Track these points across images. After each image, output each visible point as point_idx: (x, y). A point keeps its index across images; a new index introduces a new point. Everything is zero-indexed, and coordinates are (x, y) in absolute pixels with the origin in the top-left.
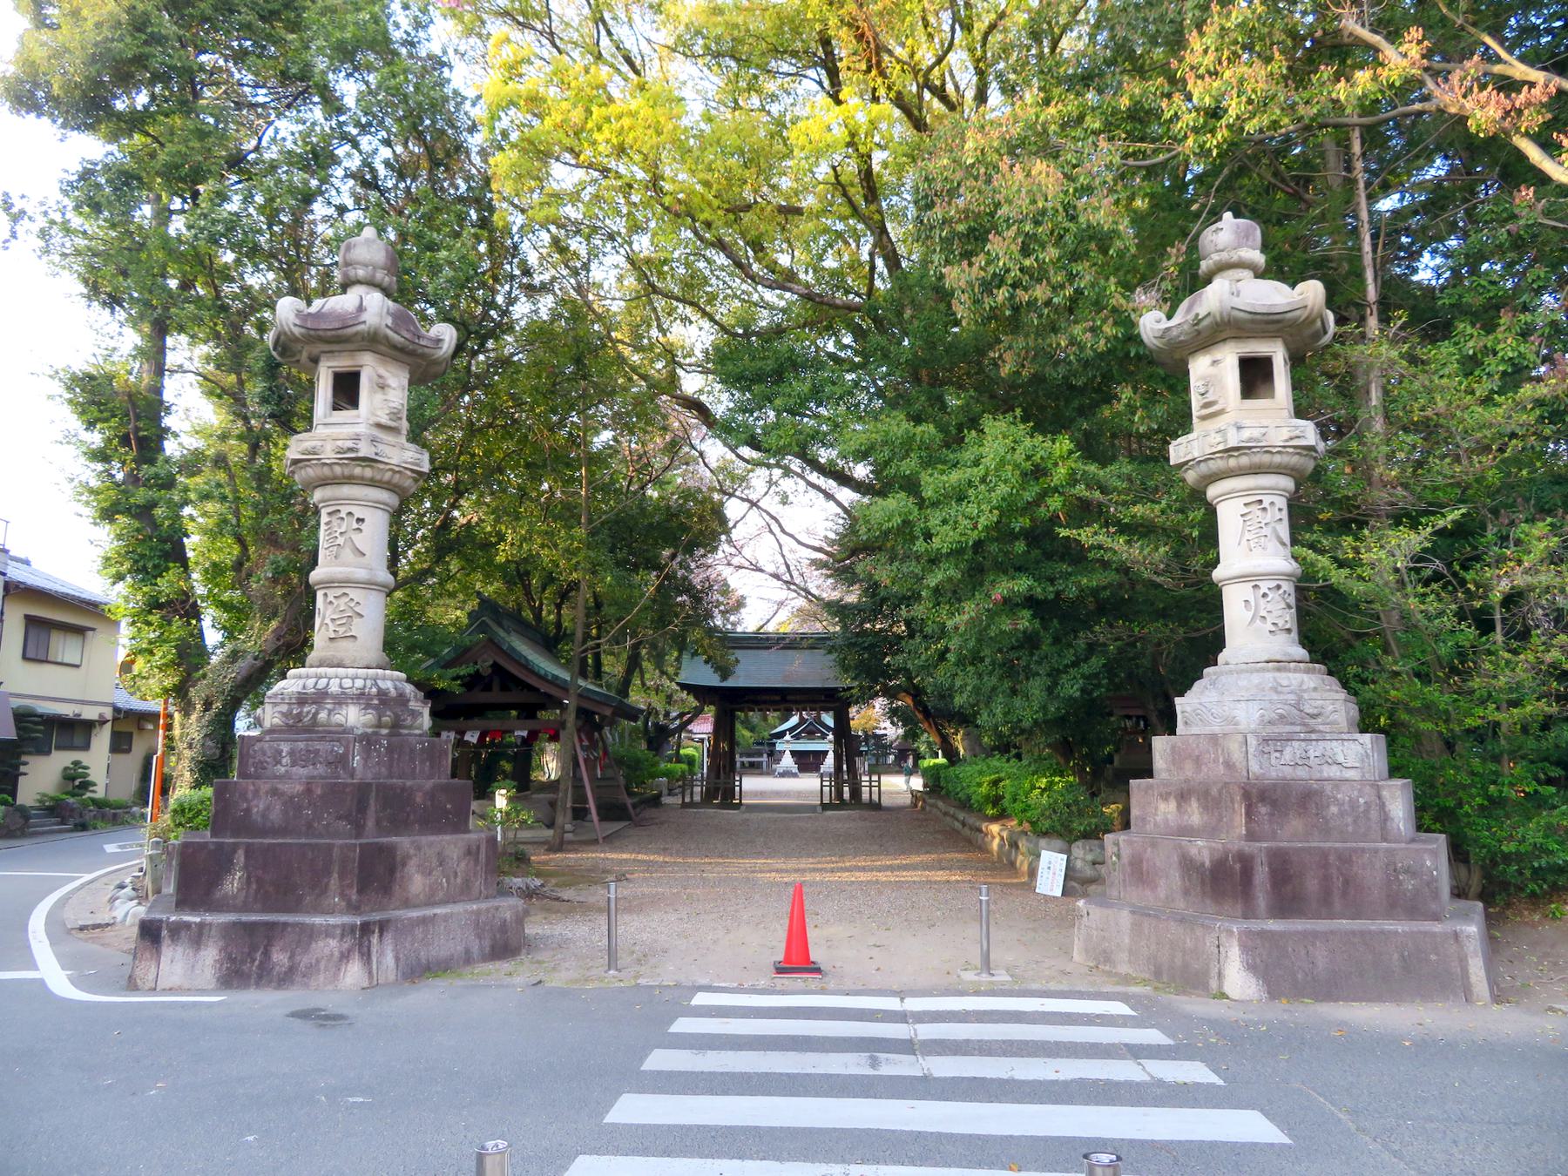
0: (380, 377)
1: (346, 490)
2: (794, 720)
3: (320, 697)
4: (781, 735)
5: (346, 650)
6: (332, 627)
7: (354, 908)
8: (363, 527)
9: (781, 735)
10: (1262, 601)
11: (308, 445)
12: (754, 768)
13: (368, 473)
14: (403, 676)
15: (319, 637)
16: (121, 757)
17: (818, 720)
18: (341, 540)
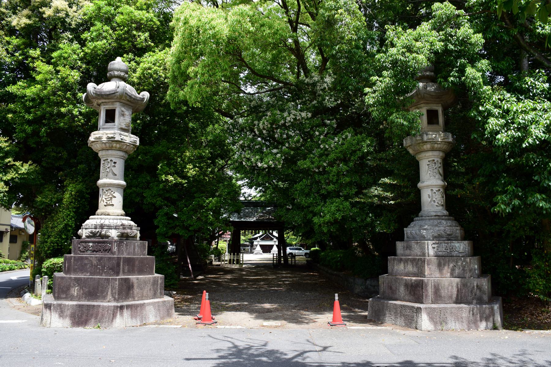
0: (122, 111)
1: (110, 152)
2: (261, 233)
3: (102, 226)
4: (256, 239)
5: (109, 210)
6: (105, 201)
7: (117, 300)
8: (116, 165)
9: (256, 239)
10: (434, 195)
11: (98, 136)
12: (247, 252)
13: (118, 146)
14: (130, 218)
15: (101, 204)
16: (14, 245)
17: (272, 234)
18: (108, 170)
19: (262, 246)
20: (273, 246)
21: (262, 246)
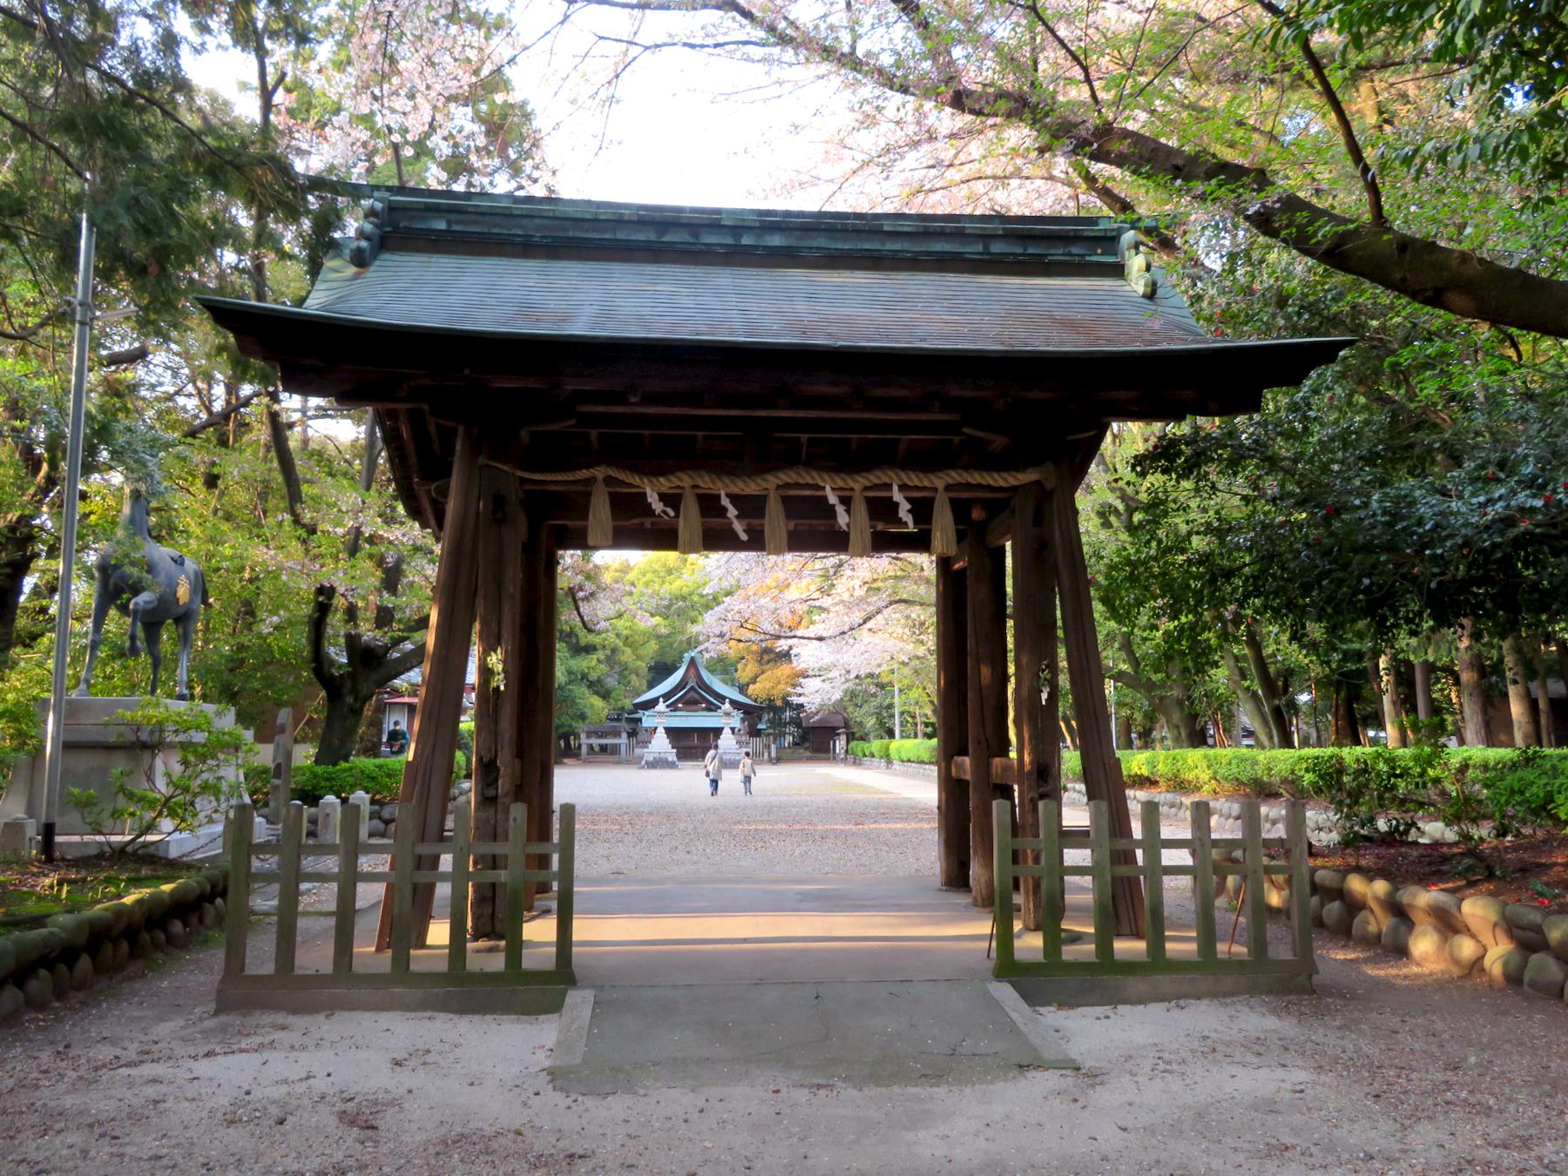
4: (651, 704)
9: (651, 704)
19: (674, 733)
20: (718, 732)
21: (674, 733)
